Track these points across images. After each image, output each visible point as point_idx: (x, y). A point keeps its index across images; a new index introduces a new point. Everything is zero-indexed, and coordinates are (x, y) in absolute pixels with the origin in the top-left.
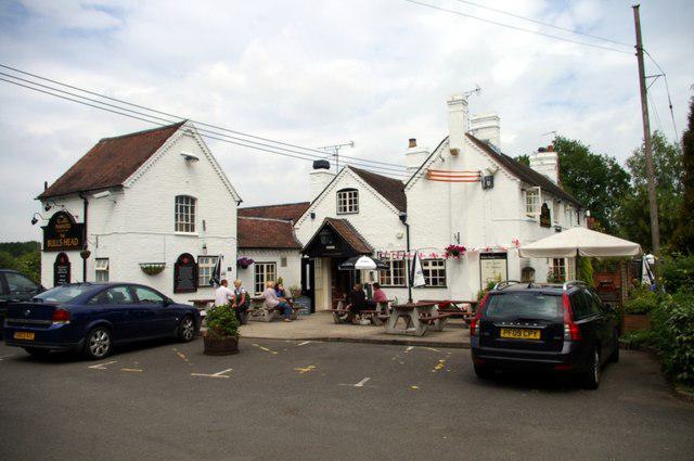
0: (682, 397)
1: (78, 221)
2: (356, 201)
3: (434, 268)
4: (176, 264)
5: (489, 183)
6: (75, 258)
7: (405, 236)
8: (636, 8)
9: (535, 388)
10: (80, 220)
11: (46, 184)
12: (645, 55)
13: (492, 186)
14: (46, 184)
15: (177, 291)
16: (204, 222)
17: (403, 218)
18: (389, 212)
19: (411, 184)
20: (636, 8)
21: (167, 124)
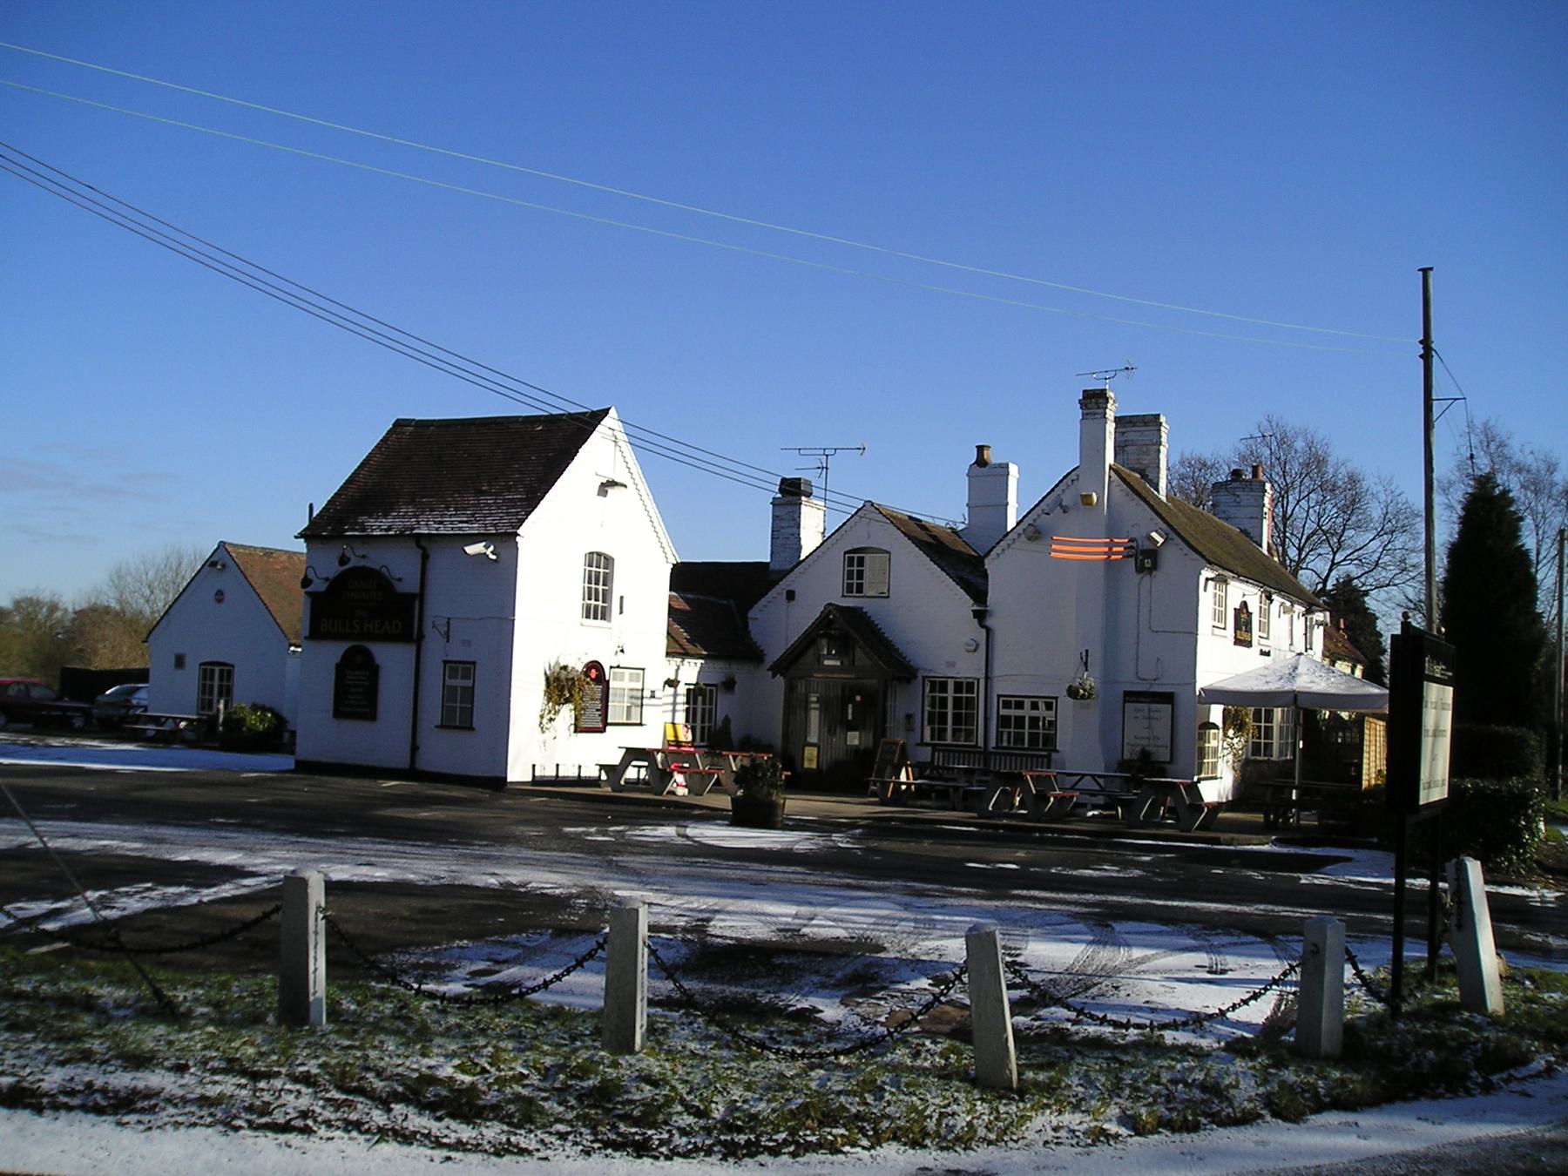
0: (731, 938)
1: (402, 588)
2: (860, 575)
3: (1019, 713)
4: (338, 665)
5: (1148, 563)
6: (392, 659)
7: (983, 647)
8: (1425, 272)
9: (110, 921)
10: (410, 585)
11: (311, 507)
12: (1435, 360)
13: (1154, 567)
14: (311, 507)
15: (1253, 755)
16: (622, 598)
17: (980, 616)
18: (952, 599)
19: (998, 550)
20: (1425, 272)
21: (555, 412)
